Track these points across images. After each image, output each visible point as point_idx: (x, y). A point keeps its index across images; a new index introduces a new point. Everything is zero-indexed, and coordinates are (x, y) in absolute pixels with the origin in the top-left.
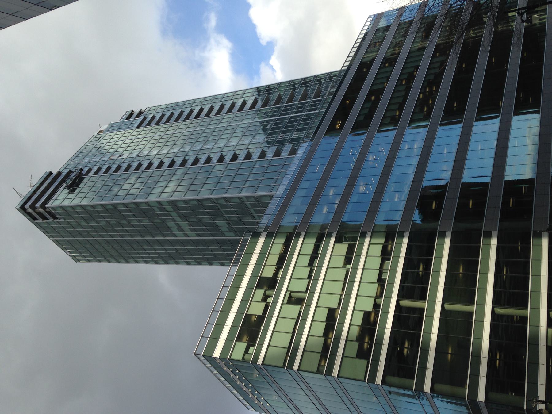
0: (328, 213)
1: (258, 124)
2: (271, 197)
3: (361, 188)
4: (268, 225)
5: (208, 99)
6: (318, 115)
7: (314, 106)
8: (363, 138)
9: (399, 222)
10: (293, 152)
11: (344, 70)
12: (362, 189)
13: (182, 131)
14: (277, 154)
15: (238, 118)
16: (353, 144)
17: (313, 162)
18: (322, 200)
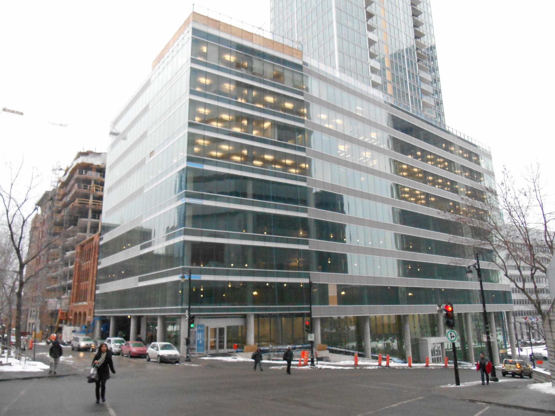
0: (321, 119)
1: (401, 48)
2: (334, 68)
3: (342, 148)
4: (309, 66)
5: (430, 18)
6: (408, 109)
7: (416, 102)
8: (384, 146)
9: (314, 178)
10: (375, 85)
11: (445, 128)
12: (341, 148)
13: (402, 18)
14: (374, 70)
15: (407, 30)
16: (379, 137)
17: (365, 103)
18: (332, 113)
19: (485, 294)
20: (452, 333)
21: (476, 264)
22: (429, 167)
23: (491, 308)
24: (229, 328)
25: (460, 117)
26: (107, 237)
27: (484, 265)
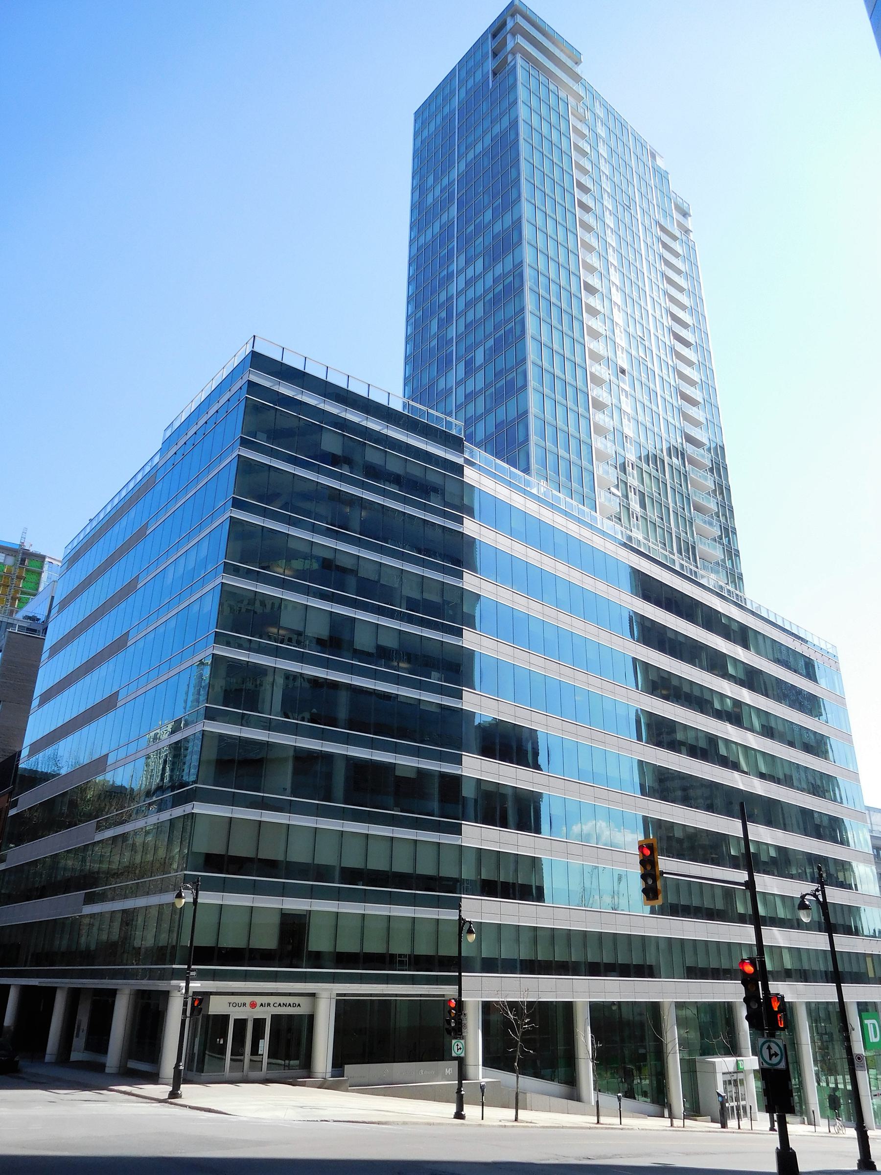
19: (838, 957)
20: (773, 1045)
21: (817, 890)
22: (763, 835)
23: (854, 993)
24: (274, 1017)
25: (783, 579)
26: (27, 800)
27: (835, 895)
